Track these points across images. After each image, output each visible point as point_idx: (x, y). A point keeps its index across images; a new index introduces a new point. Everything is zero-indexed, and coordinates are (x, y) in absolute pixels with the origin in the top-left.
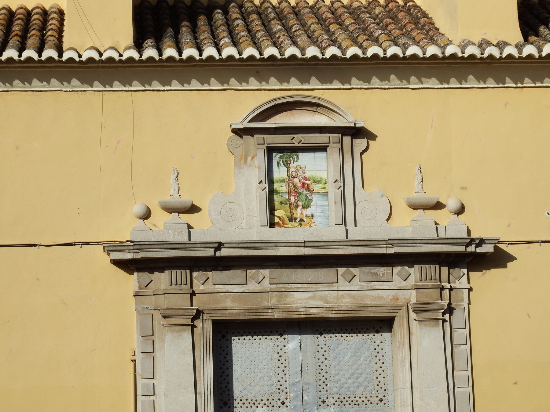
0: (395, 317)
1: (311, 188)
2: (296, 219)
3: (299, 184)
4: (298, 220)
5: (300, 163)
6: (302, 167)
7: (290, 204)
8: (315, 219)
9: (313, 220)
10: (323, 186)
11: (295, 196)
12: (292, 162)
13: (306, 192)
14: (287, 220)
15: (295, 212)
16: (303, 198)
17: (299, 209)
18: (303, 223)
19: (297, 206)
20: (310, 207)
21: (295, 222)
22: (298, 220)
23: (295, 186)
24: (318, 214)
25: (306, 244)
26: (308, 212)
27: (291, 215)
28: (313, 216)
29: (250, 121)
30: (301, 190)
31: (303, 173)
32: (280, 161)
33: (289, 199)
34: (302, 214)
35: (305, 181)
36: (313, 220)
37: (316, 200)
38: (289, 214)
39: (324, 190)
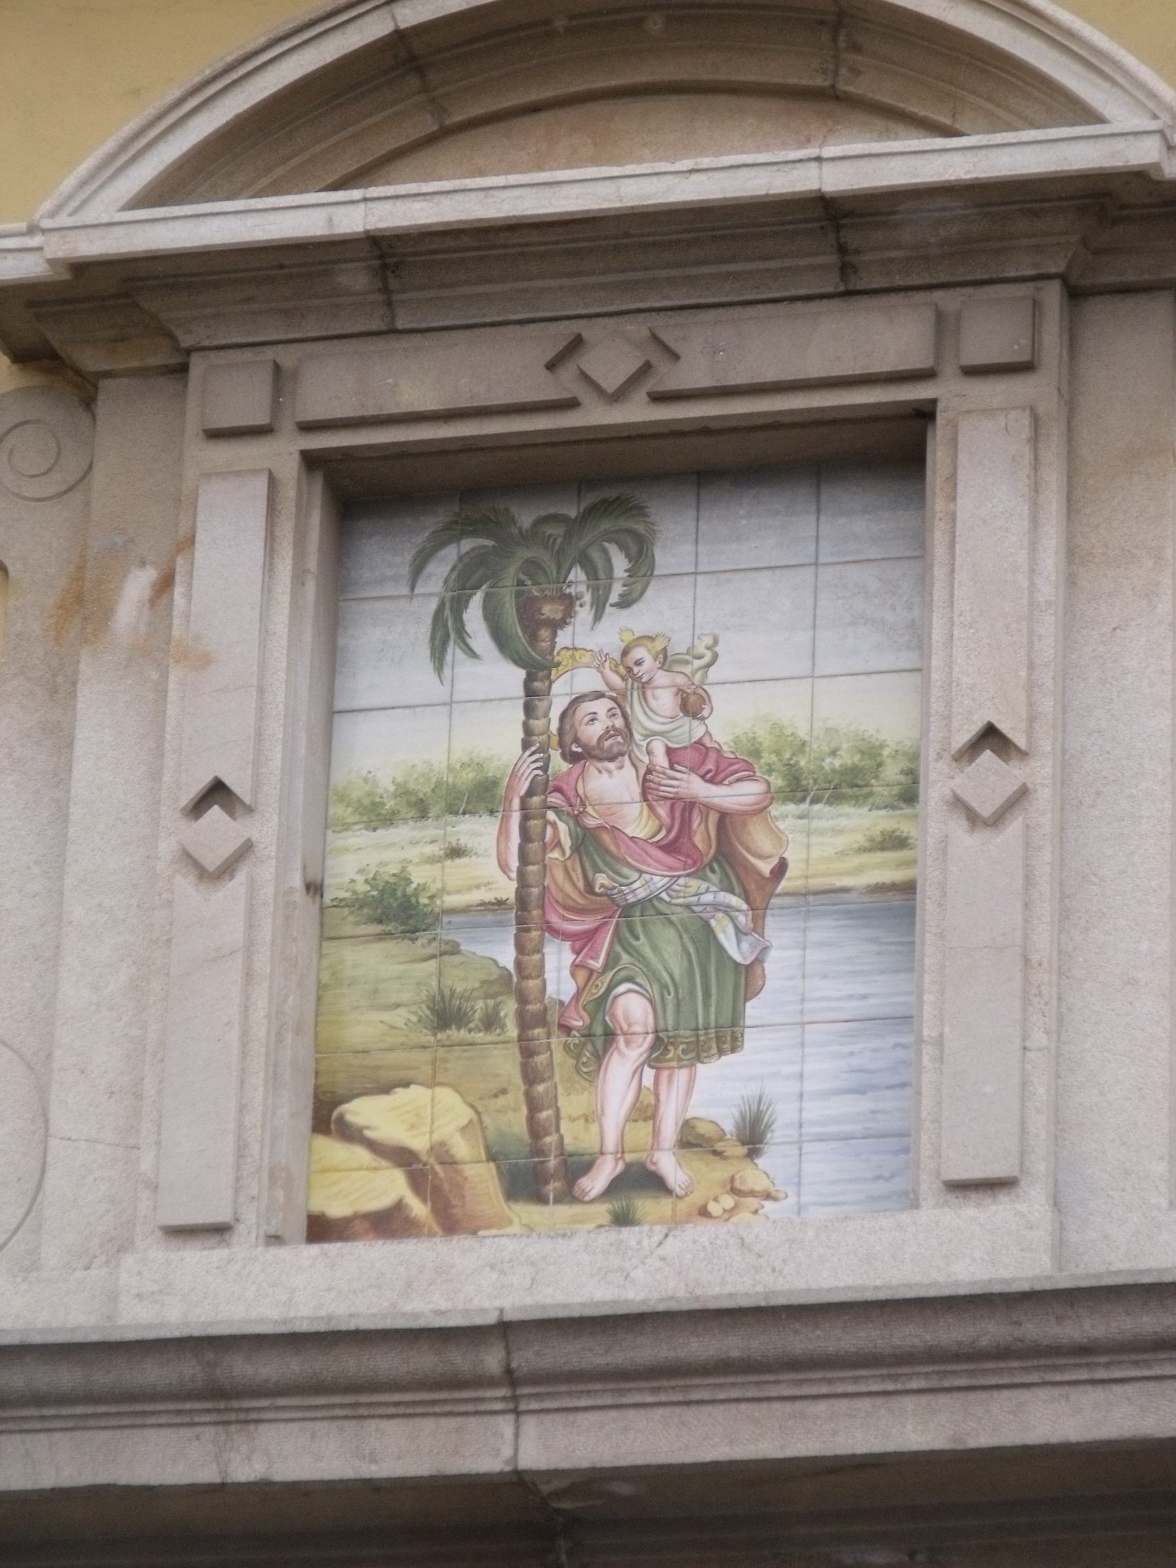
0: (934, 402)
1: (758, 849)
2: (577, 1167)
3: (638, 823)
4: (596, 1182)
5: (663, 613)
6: (679, 645)
7: (525, 1022)
8: (774, 1162)
9: (752, 1177)
10: (880, 821)
11: (583, 941)
12: (584, 614)
13: (706, 892)
14: (482, 1180)
15: (571, 1104)
16: (668, 951)
17: (621, 1074)
18: (646, 1205)
19: (601, 1039)
20: (727, 1038)
21: (568, 1196)
22: (596, 1182)
23: (591, 844)
24: (814, 1111)
25: (526, 1358)
26: (713, 1091)
27: (536, 1131)
28: (753, 1136)
29: (171, 189)
30: (649, 880)
31: (692, 705)
32: (459, 605)
33: (528, 966)
34: (645, 1111)
35: (696, 787)
36: (752, 1177)
37: (805, 976)
38: (516, 1122)
39: (883, 870)
